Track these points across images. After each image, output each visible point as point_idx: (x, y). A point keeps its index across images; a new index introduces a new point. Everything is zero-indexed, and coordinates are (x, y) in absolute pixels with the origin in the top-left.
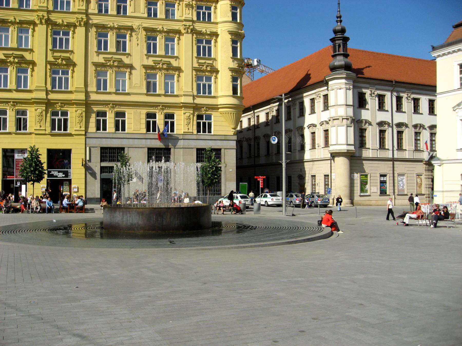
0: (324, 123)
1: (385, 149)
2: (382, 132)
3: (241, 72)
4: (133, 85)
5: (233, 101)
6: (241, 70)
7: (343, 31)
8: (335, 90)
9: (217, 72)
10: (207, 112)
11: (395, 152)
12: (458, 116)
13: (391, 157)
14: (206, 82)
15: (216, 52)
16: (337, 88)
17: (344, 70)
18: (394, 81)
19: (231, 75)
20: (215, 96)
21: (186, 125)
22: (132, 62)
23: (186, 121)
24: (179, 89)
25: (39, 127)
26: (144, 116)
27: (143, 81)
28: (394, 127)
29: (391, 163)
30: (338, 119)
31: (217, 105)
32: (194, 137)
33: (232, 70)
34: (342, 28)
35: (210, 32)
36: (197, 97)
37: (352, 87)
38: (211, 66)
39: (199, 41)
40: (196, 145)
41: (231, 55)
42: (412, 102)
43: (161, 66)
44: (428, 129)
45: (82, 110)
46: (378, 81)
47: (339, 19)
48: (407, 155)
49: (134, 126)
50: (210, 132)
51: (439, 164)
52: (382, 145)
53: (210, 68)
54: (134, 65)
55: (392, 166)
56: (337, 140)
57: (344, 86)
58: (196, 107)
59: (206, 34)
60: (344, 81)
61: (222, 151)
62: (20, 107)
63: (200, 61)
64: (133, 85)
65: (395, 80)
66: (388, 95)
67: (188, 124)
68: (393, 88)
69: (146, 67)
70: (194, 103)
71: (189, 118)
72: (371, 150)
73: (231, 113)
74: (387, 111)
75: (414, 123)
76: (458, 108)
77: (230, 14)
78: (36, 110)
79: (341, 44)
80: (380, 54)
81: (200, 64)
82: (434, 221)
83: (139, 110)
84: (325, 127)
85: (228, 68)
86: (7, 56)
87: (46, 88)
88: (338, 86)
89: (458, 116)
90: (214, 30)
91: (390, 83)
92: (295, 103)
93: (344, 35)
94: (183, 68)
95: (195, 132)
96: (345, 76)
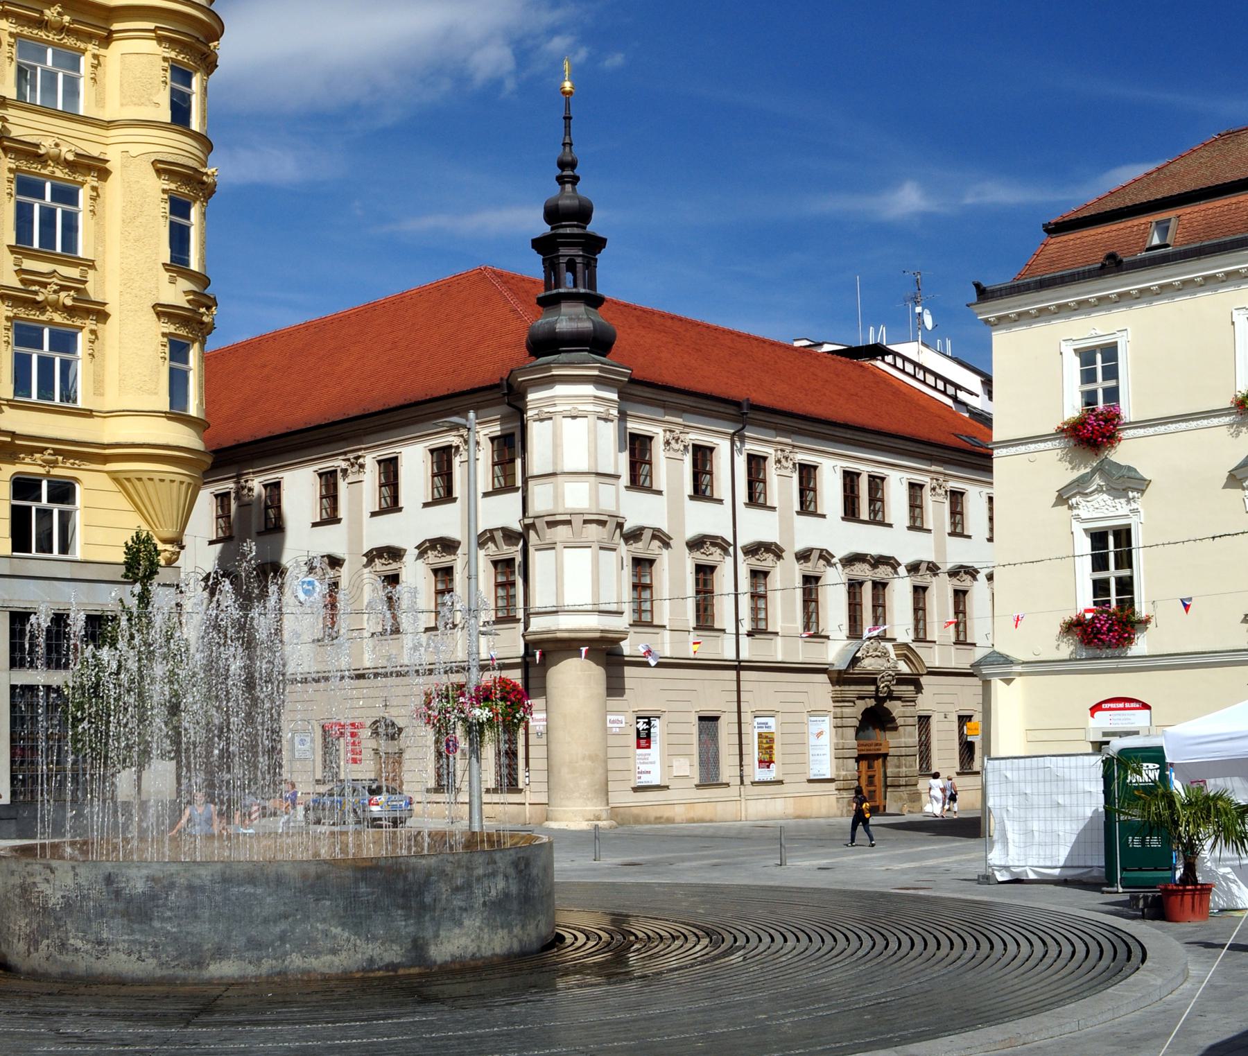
0: (499, 536)
1: (712, 629)
2: (704, 572)
6: (205, 319)
7: (583, 214)
8: (592, 418)
9: (100, 314)
10: (55, 472)
11: (744, 640)
12: (1077, 517)
13: (733, 657)
14: (53, 354)
15: (100, 238)
17: (590, 352)
18: (745, 405)
20: (91, 411)
28: (740, 553)
29: (732, 674)
30: (569, 522)
33: (163, 312)
34: (580, 205)
35: (77, 155)
36: (12, 407)
37: (615, 412)
38: (77, 290)
39: (27, 187)
41: (165, 255)
42: (796, 476)
44: (839, 566)
46: (692, 399)
47: (567, 171)
48: (778, 651)
50: (64, 548)
52: (705, 619)
56: (559, 592)
59: (58, 160)
63: (28, 264)
65: (748, 399)
66: (723, 447)
72: (667, 634)
74: (720, 501)
75: (800, 546)
77: (164, 98)
80: (653, 313)
84: (810, 568)
88: (568, 408)
89: (1077, 517)
90: (94, 151)
92: (361, 461)
93: (585, 228)
96: (596, 373)
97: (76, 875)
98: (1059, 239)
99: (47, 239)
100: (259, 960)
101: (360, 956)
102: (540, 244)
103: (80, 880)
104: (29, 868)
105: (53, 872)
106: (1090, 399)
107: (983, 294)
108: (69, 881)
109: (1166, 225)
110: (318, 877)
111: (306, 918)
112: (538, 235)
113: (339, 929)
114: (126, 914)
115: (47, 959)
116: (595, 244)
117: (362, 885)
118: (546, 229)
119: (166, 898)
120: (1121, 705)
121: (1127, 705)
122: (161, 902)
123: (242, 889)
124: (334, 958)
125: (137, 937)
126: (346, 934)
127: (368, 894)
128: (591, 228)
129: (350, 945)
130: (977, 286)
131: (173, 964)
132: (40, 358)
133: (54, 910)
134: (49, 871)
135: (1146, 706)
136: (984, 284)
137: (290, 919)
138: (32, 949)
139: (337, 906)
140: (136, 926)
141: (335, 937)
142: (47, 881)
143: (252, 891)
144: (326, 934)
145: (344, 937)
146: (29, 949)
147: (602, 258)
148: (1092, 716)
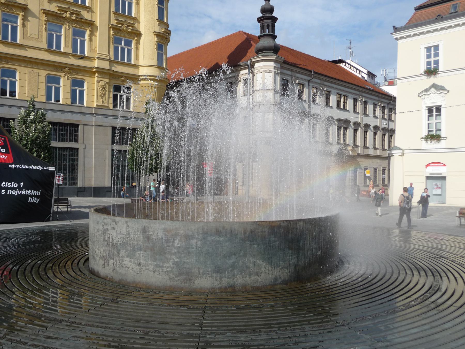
3: (167, 39)
4: (29, 35)
5: (154, 72)
7: (272, 10)
8: (263, 73)
9: (139, 35)
14: (125, 47)
15: (138, 11)
16: (266, 71)
17: (273, 53)
19: (156, 41)
21: (100, 96)
22: (28, 3)
23: (100, 92)
24: (90, 50)
25: (101, 102)
26: (43, 79)
27: (42, 32)
31: (139, 76)
32: (110, 113)
33: (157, 34)
40: (111, 122)
41: (157, 16)
43: (68, 16)
45: (105, 81)
49: (28, 91)
51: (400, 154)
53: (131, 29)
54: (29, 7)
55: (388, 162)
57: (273, 70)
58: (111, 75)
60: (272, 64)
61: (81, 128)
62: (118, 83)
64: (29, 35)
67: (103, 96)
68: (311, 78)
69: (47, 13)
70: (110, 70)
71: (104, 88)
73: (152, 87)
76: (425, 94)
78: (98, 82)
79: (270, 24)
81: (119, 22)
82: (407, 211)
83: (36, 71)
85: (152, 32)
86: (60, 9)
87: (110, 58)
88: (267, 69)
91: (309, 73)
94: (98, 23)
95: (111, 106)
97: (128, 226)
98: (419, 12)
99: (123, 58)
100: (221, 278)
101: (270, 276)
102: (259, 20)
103: (129, 229)
104: (105, 221)
105: (116, 224)
106: (429, 63)
107: (396, 29)
108: (124, 229)
109: (456, 6)
110: (252, 232)
111: (245, 255)
112: (259, 17)
113: (261, 261)
114: (152, 249)
115: (113, 271)
116: (275, 19)
117: (273, 236)
118: (261, 15)
119: (174, 242)
120: (436, 165)
121: (438, 165)
122: (171, 244)
123: (213, 238)
124: (258, 278)
125: (158, 263)
126: (264, 264)
127: (276, 241)
128: (274, 15)
129: (266, 271)
130: (394, 27)
131: (177, 279)
132: (121, 48)
133: (116, 245)
134: (114, 223)
135: (445, 165)
136: (397, 27)
137: (237, 255)
138: (106, 264)
139: (260, 248)
140: (157, 257)
141: (259, 266)
142: (114, 228)
143: (218, 239)
144: (255, 264)
145: (263, 266)
146: (104, 264)
147: (277, 24)
148: (426, 168)
